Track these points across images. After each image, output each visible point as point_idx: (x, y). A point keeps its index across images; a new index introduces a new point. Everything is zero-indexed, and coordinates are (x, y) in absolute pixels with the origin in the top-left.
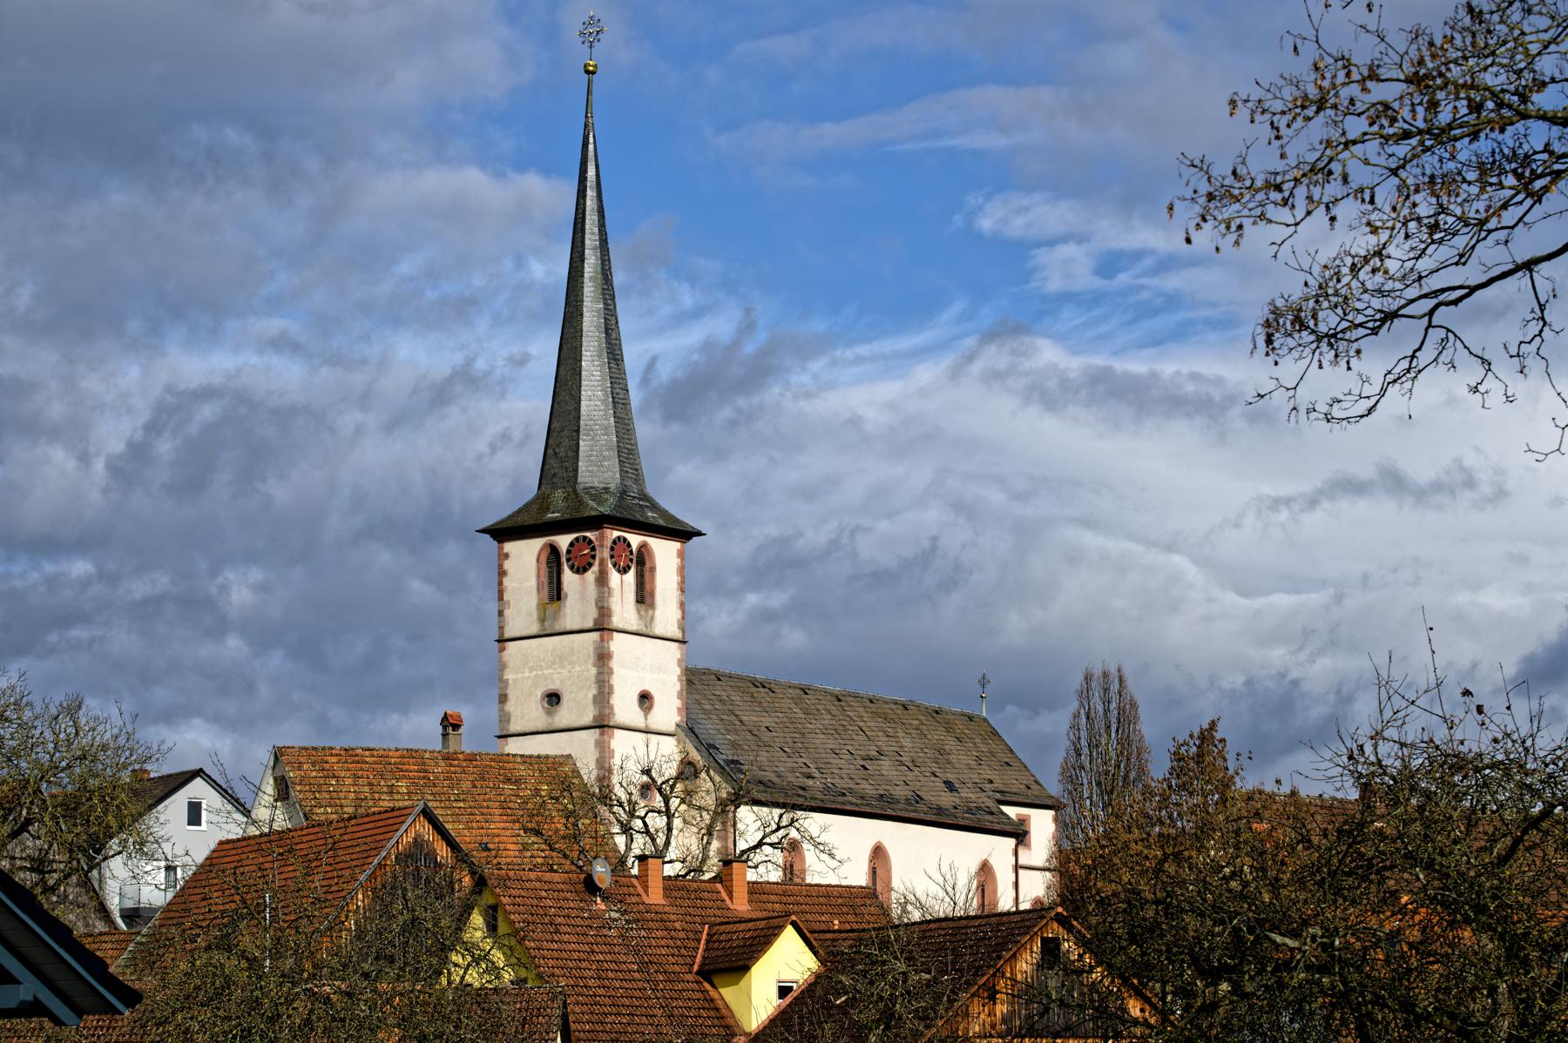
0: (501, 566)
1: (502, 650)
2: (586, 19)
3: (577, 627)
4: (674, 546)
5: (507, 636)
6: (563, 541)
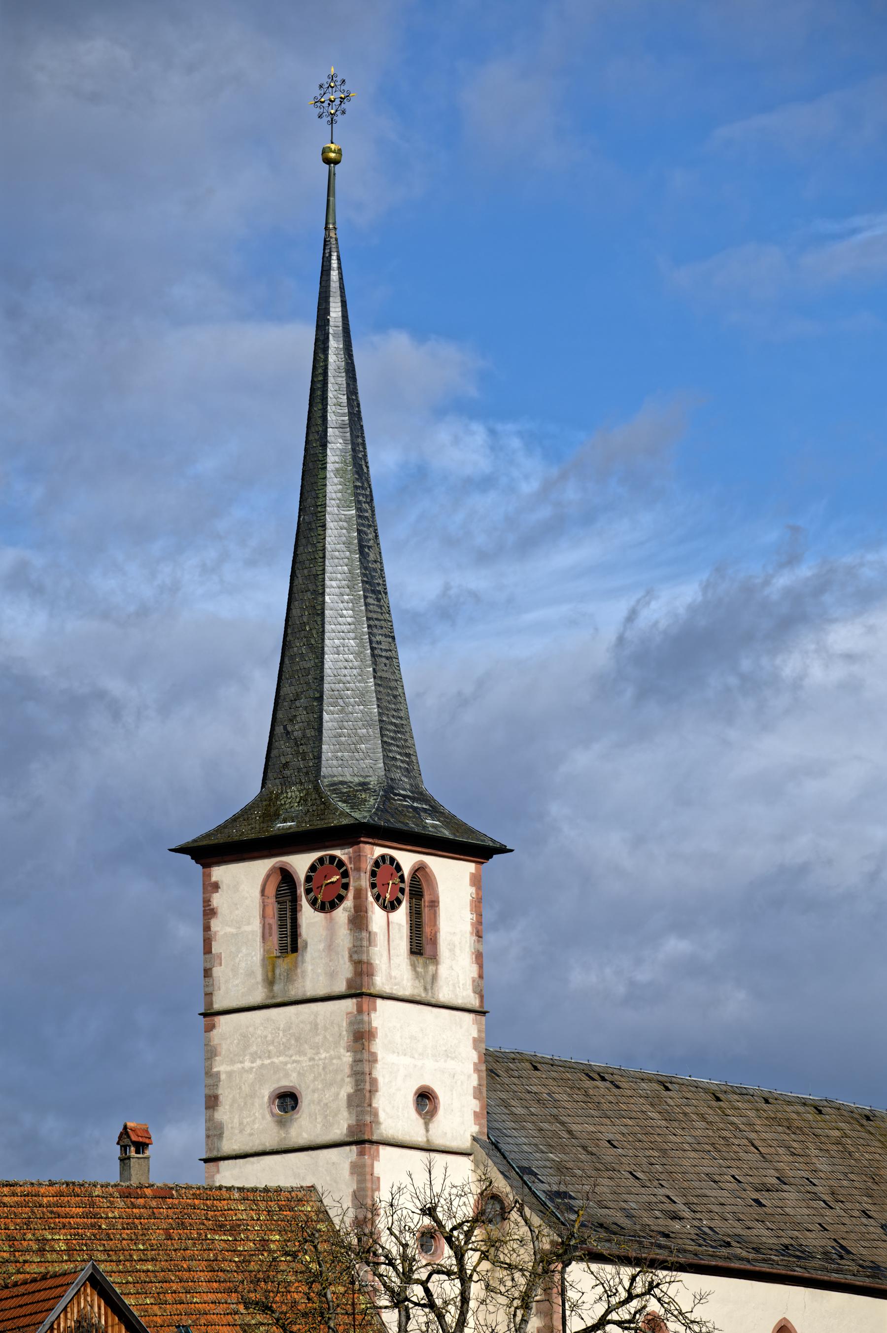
0: (207, 902)
1: (210, 1028)
2: (325, 80)
3: (322, 992)
4: (466, 868)
6: (300, 863)
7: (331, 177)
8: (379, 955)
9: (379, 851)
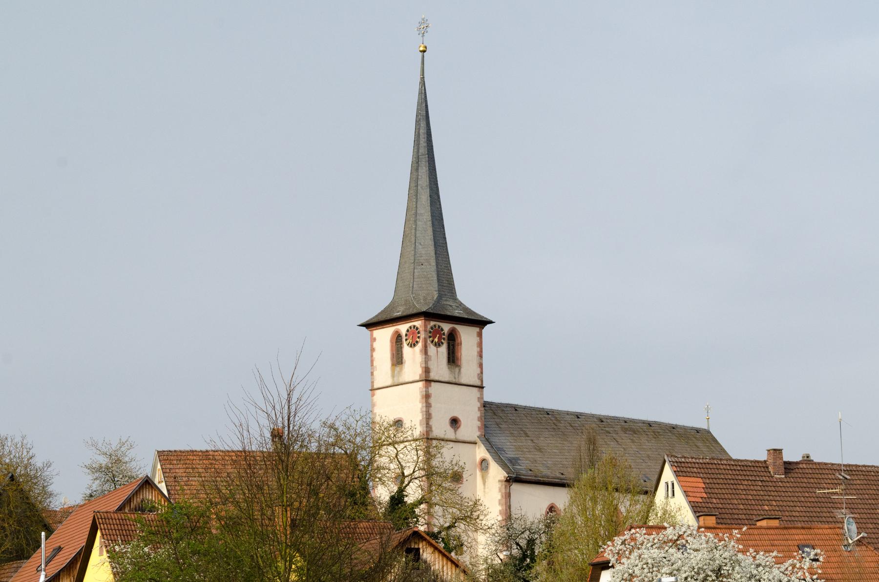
0: (372, 345)
1: (373, 395)
2: (421, 20)
3: (411, 380)
4: (475, 330)
5: (375, 387)
6: (403, 328)
7: (423, 56)
8: (432, 365)
9: (432, 323)
